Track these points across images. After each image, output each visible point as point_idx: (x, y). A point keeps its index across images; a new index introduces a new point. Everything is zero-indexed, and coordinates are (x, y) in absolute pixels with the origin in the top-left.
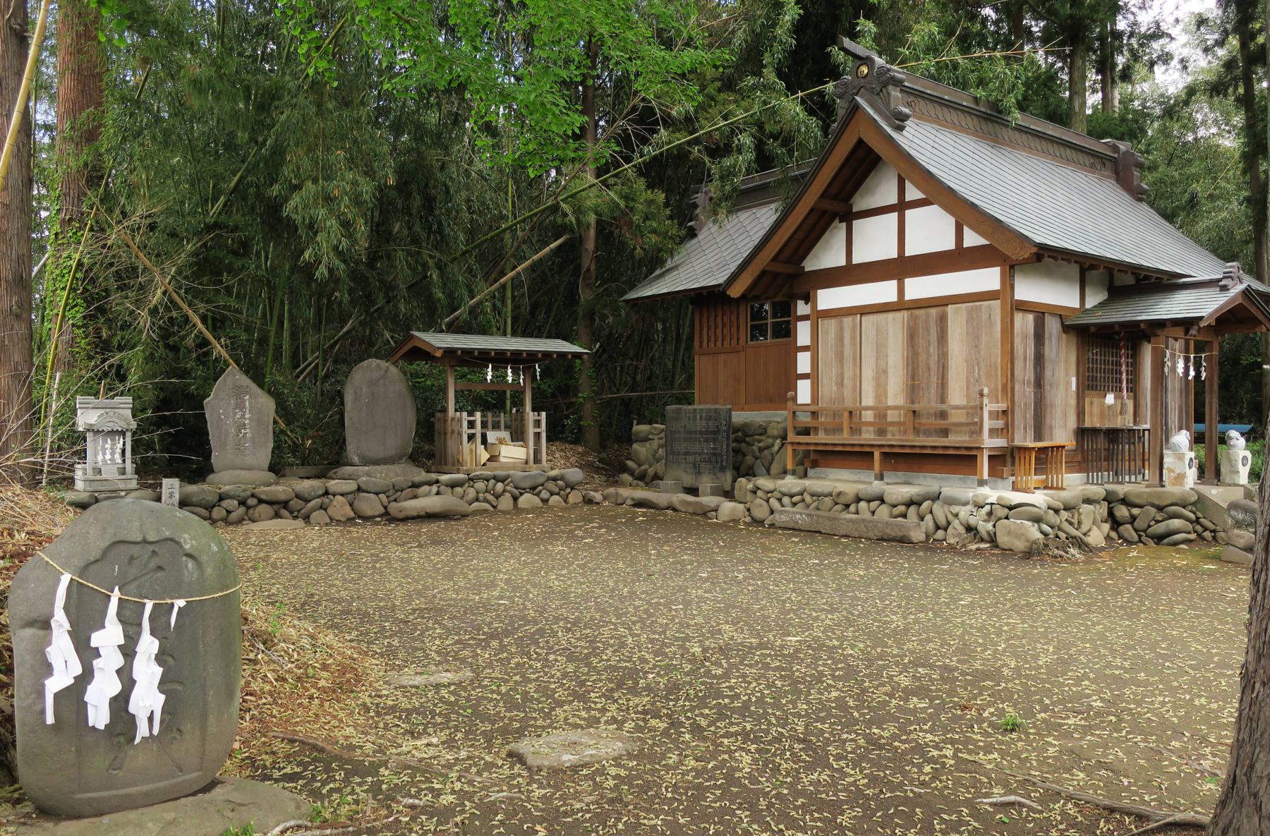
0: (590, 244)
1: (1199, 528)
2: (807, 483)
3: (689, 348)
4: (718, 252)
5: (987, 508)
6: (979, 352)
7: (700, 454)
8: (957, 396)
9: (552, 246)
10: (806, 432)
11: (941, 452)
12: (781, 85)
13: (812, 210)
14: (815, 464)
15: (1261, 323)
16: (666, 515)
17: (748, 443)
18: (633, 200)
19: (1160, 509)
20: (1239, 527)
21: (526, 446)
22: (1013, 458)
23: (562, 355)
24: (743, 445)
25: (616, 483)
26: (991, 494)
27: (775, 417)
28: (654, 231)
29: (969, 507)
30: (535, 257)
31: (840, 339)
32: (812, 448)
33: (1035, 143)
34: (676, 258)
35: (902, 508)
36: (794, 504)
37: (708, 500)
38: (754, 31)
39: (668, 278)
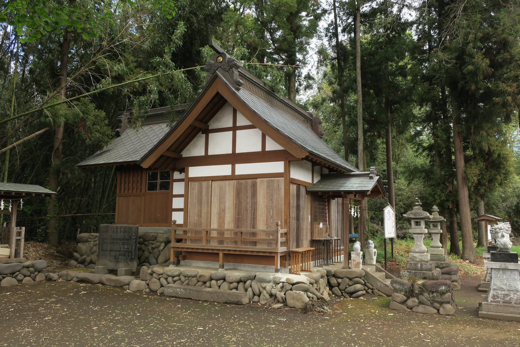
0: (60, 134)
1: (366, 288)
2: (182, 269)
3: (115, 193)
4: (136, 143)
5: (281, 284)
6: (273, 203)
7: (119, 251)
8: (261, 225)
9: (37, 133)
10: (179, 241)
11: (256, 254)
12: (172, 64)
13: (190, 125)
14: (184, 258)
15: (380, 193)
16: (98, 288)
17: (146, 245)
18: (87, 114)
19: (350, 279)
20: (396, 292)
21: (10, 247)
22: (290, 256)
23: (38, 194)
24: (143, 246)
25: (67, 266)
26: (284, 276)
27: (160, 231)
28: (97, 131)
29: (271, 284)
30: (26, 139)
31: (200, 192)
32: (185, 250)
33: (285, 108)
34: (108, 146)
35: (235, 284)
36: (175, 282)
37: (125, 279)
38: (154, 43)
39: (104, 156)
